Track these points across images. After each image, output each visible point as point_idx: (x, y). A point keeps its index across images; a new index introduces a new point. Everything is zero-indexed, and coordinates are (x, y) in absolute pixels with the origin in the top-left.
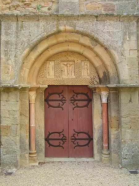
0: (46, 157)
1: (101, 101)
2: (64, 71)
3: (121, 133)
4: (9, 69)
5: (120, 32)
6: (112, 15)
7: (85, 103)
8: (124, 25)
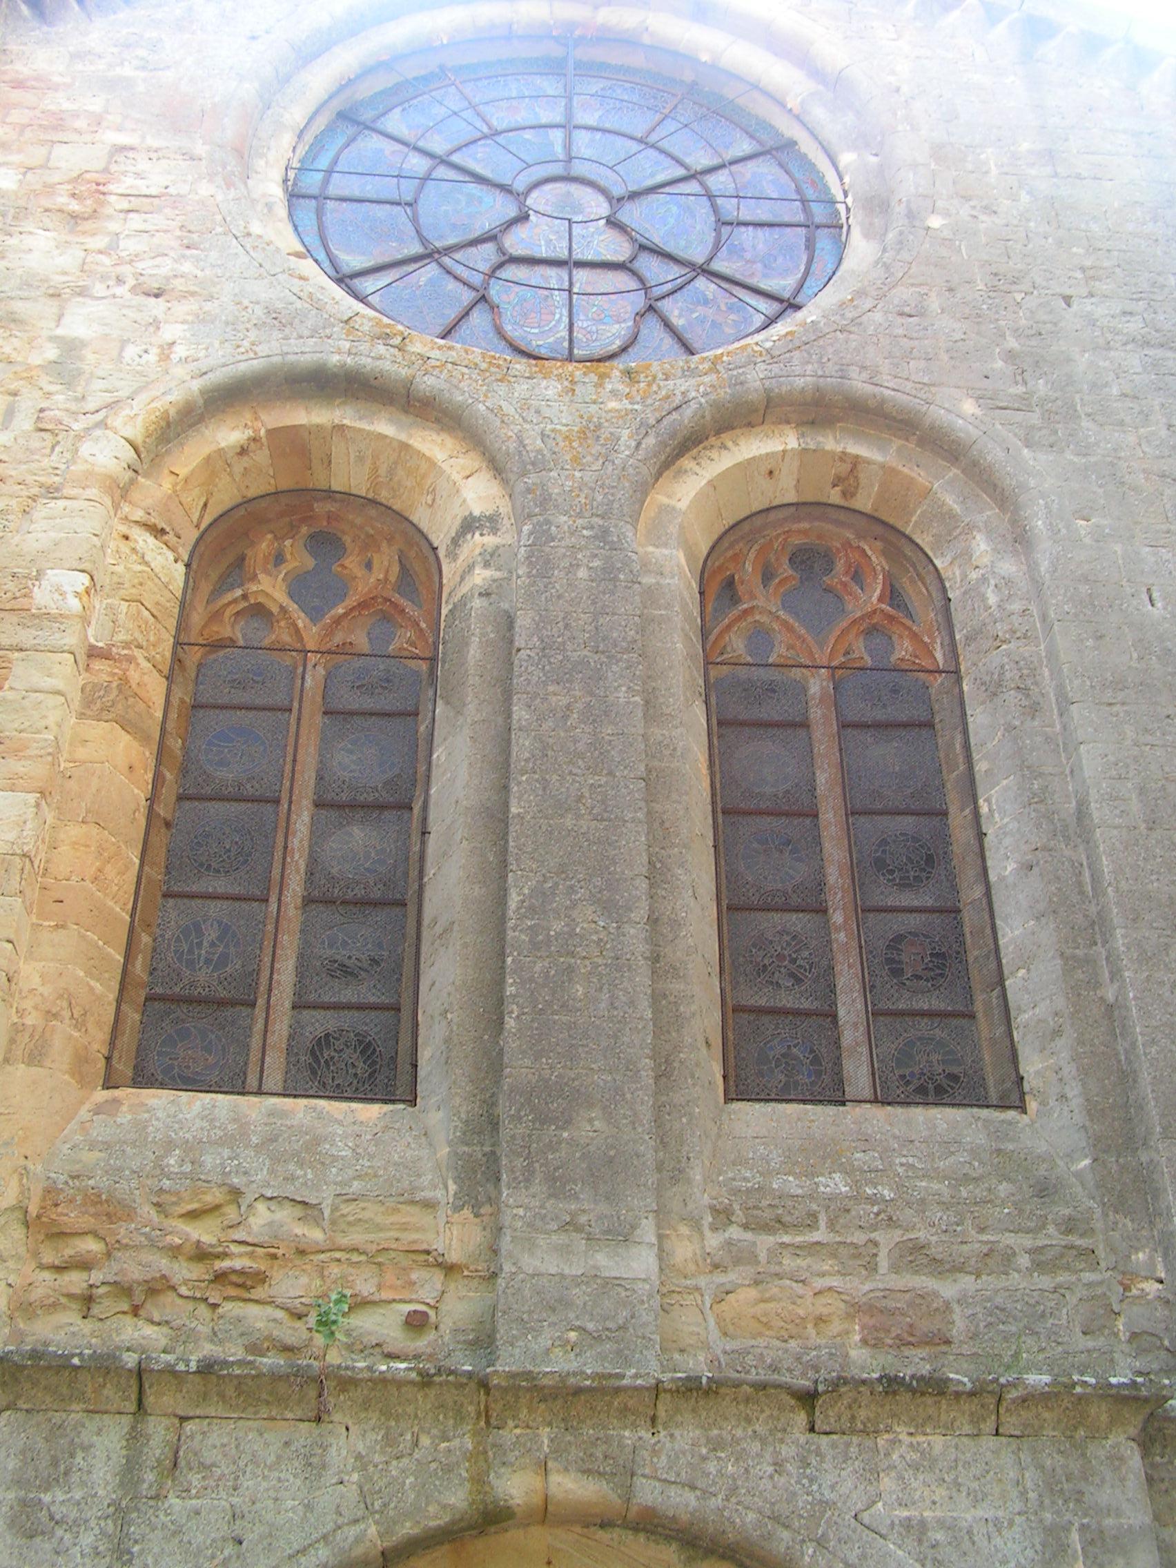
5: (1011, 1523)
6: (933, 1387)
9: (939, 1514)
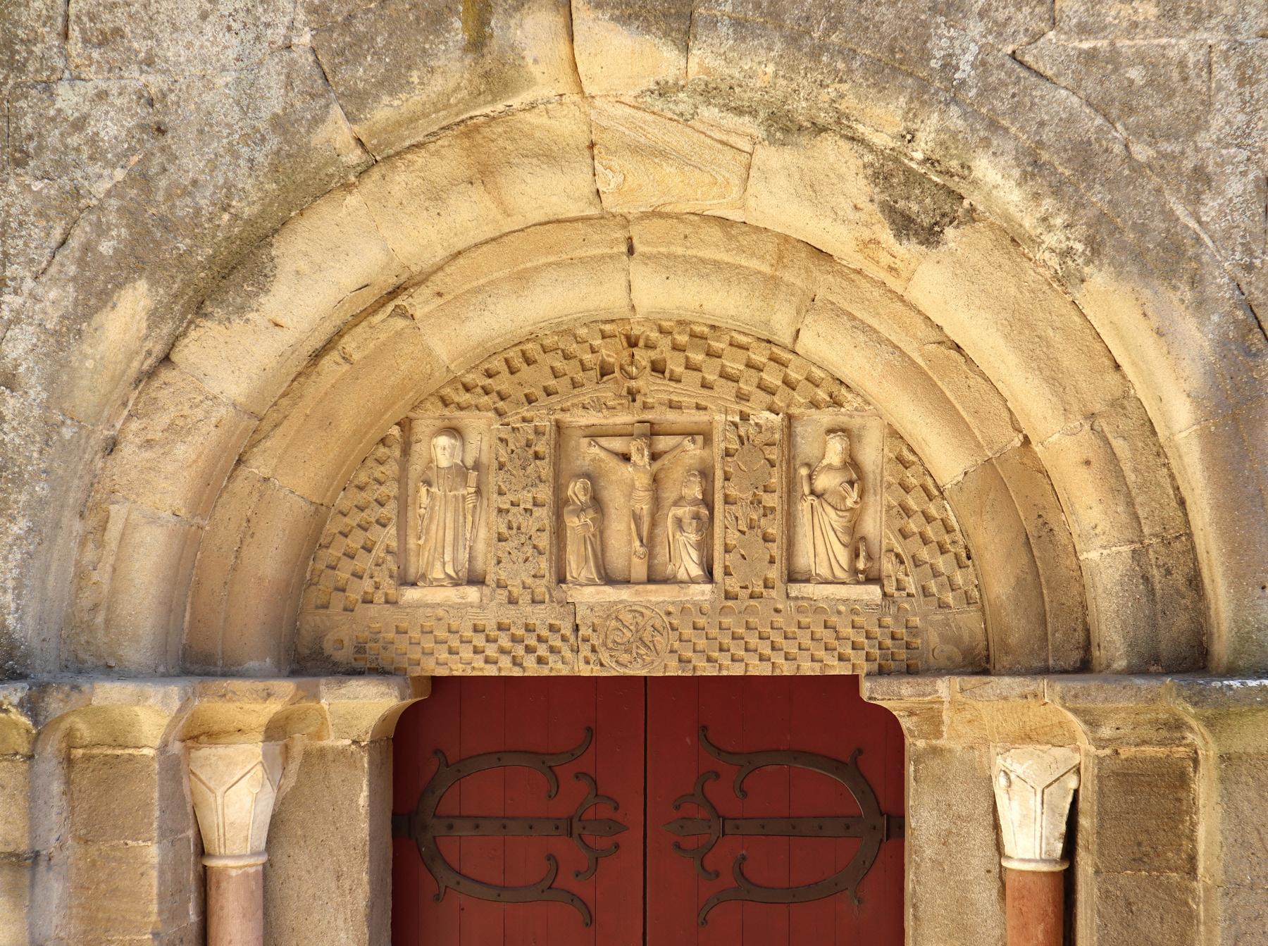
9: (1139, 41)
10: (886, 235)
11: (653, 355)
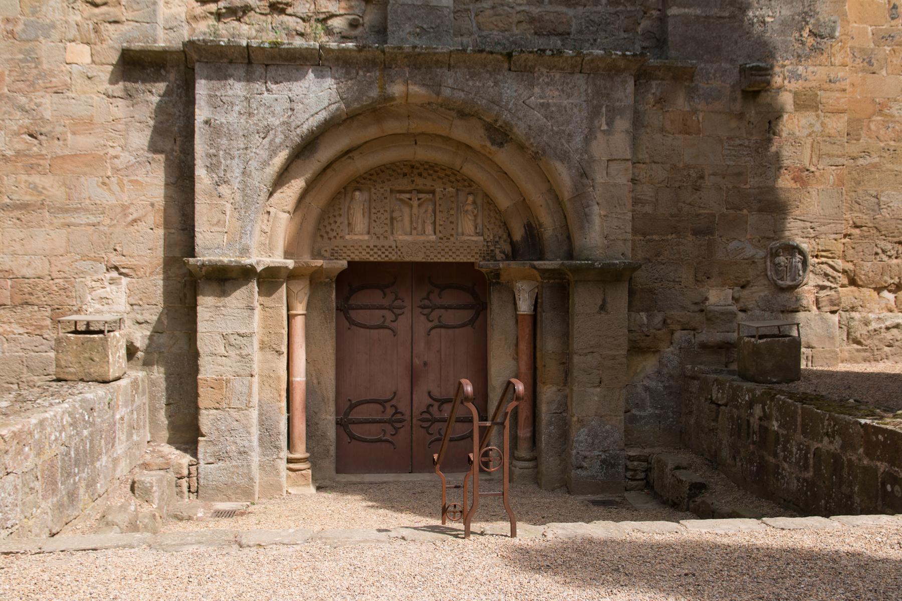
0: (338, 471)
1: (516, 309)
2: (402, 220)
3: (572, 398)
4: (224, 213)
7: (465, 315)
8: (595, 85)
10: (489, 144)
11: (419, 171)
